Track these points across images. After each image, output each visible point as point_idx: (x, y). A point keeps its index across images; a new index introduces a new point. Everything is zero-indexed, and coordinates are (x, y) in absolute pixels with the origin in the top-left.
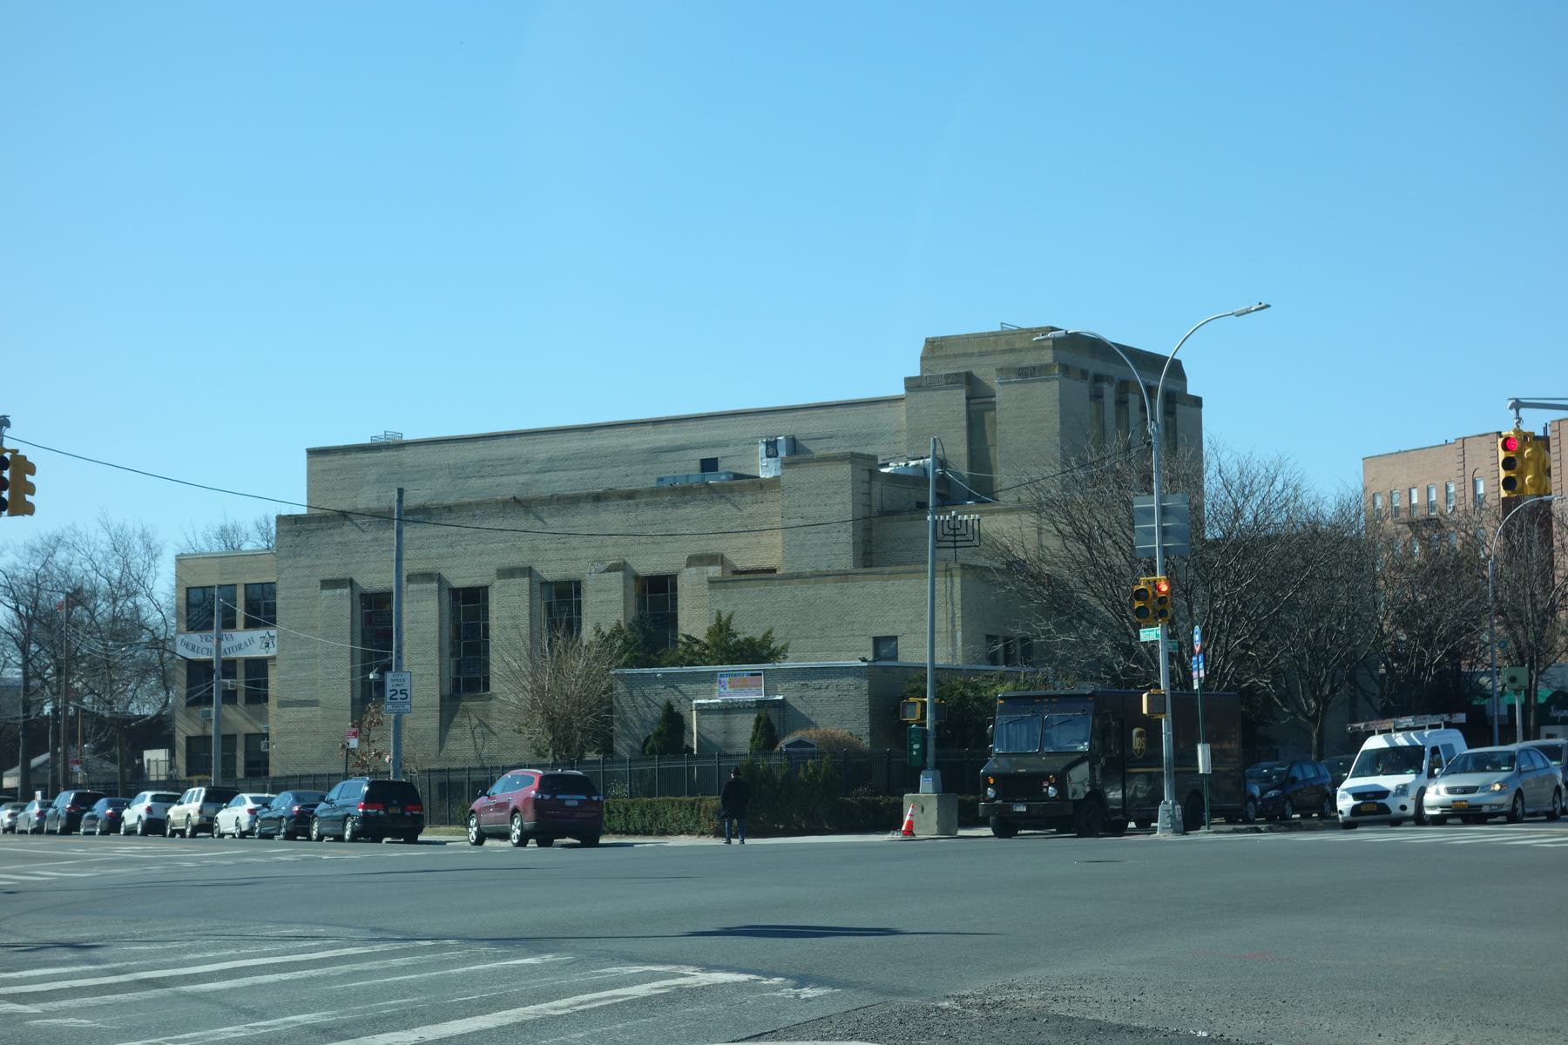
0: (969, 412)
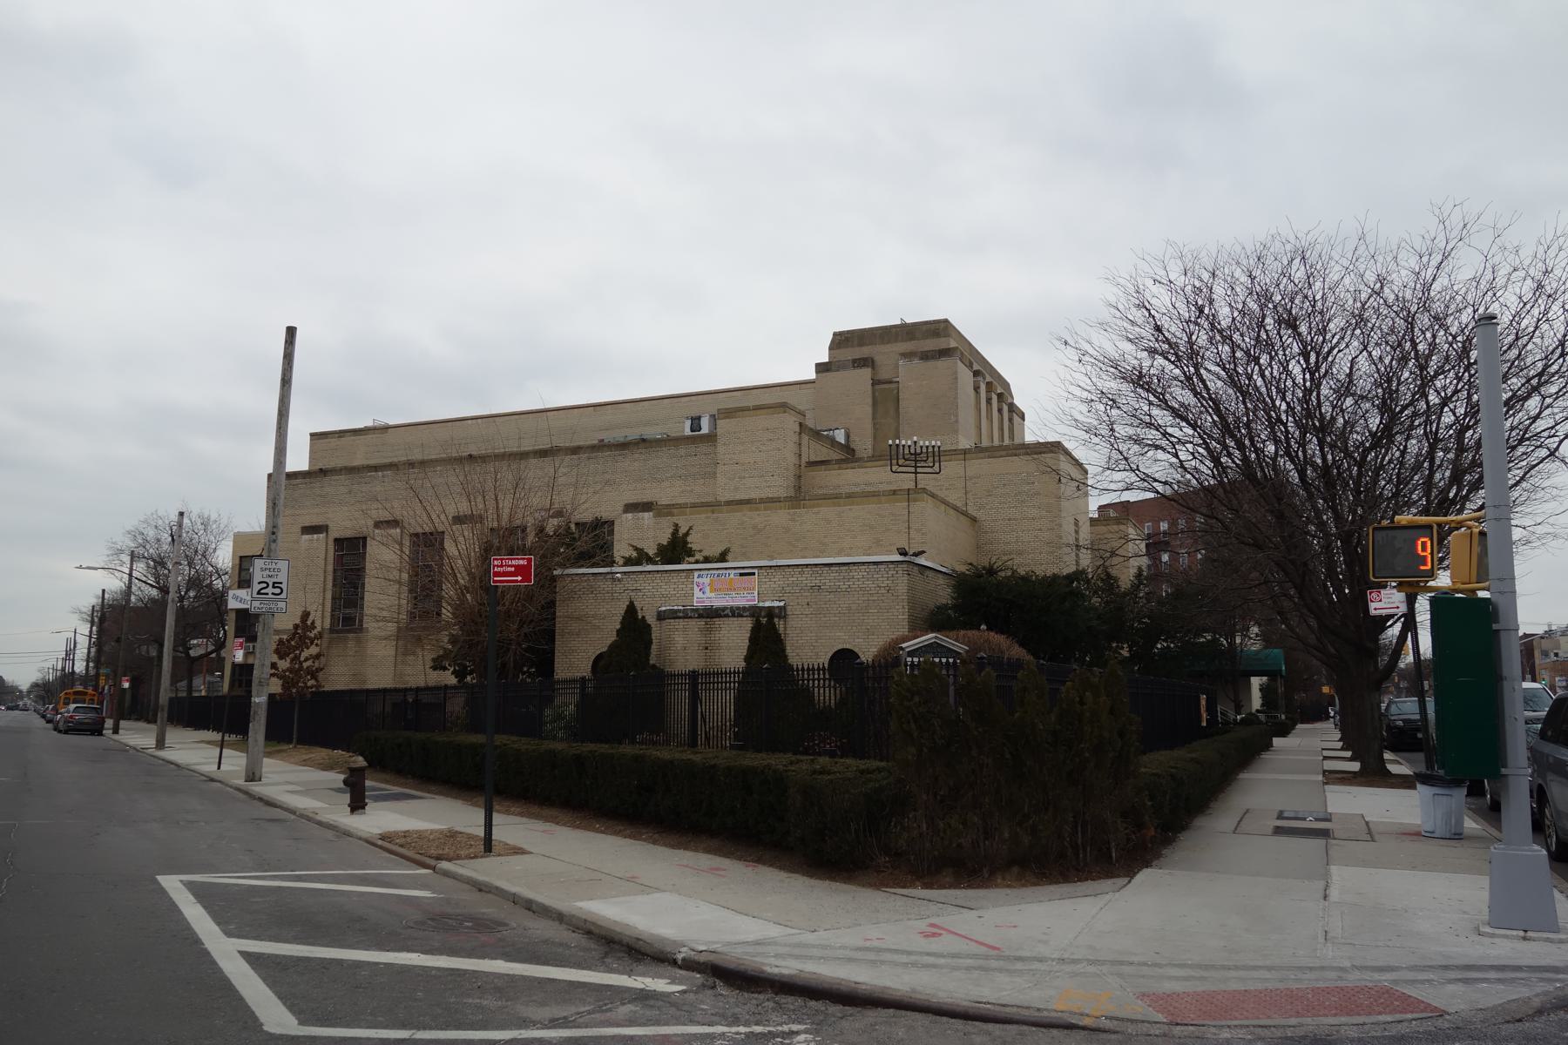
0: (553, 641)
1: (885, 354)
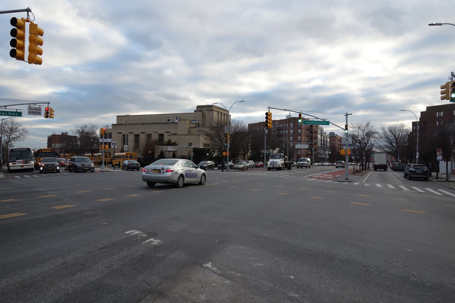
1: (204, 109)
